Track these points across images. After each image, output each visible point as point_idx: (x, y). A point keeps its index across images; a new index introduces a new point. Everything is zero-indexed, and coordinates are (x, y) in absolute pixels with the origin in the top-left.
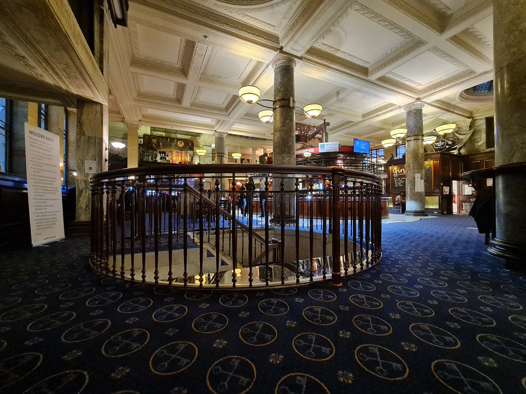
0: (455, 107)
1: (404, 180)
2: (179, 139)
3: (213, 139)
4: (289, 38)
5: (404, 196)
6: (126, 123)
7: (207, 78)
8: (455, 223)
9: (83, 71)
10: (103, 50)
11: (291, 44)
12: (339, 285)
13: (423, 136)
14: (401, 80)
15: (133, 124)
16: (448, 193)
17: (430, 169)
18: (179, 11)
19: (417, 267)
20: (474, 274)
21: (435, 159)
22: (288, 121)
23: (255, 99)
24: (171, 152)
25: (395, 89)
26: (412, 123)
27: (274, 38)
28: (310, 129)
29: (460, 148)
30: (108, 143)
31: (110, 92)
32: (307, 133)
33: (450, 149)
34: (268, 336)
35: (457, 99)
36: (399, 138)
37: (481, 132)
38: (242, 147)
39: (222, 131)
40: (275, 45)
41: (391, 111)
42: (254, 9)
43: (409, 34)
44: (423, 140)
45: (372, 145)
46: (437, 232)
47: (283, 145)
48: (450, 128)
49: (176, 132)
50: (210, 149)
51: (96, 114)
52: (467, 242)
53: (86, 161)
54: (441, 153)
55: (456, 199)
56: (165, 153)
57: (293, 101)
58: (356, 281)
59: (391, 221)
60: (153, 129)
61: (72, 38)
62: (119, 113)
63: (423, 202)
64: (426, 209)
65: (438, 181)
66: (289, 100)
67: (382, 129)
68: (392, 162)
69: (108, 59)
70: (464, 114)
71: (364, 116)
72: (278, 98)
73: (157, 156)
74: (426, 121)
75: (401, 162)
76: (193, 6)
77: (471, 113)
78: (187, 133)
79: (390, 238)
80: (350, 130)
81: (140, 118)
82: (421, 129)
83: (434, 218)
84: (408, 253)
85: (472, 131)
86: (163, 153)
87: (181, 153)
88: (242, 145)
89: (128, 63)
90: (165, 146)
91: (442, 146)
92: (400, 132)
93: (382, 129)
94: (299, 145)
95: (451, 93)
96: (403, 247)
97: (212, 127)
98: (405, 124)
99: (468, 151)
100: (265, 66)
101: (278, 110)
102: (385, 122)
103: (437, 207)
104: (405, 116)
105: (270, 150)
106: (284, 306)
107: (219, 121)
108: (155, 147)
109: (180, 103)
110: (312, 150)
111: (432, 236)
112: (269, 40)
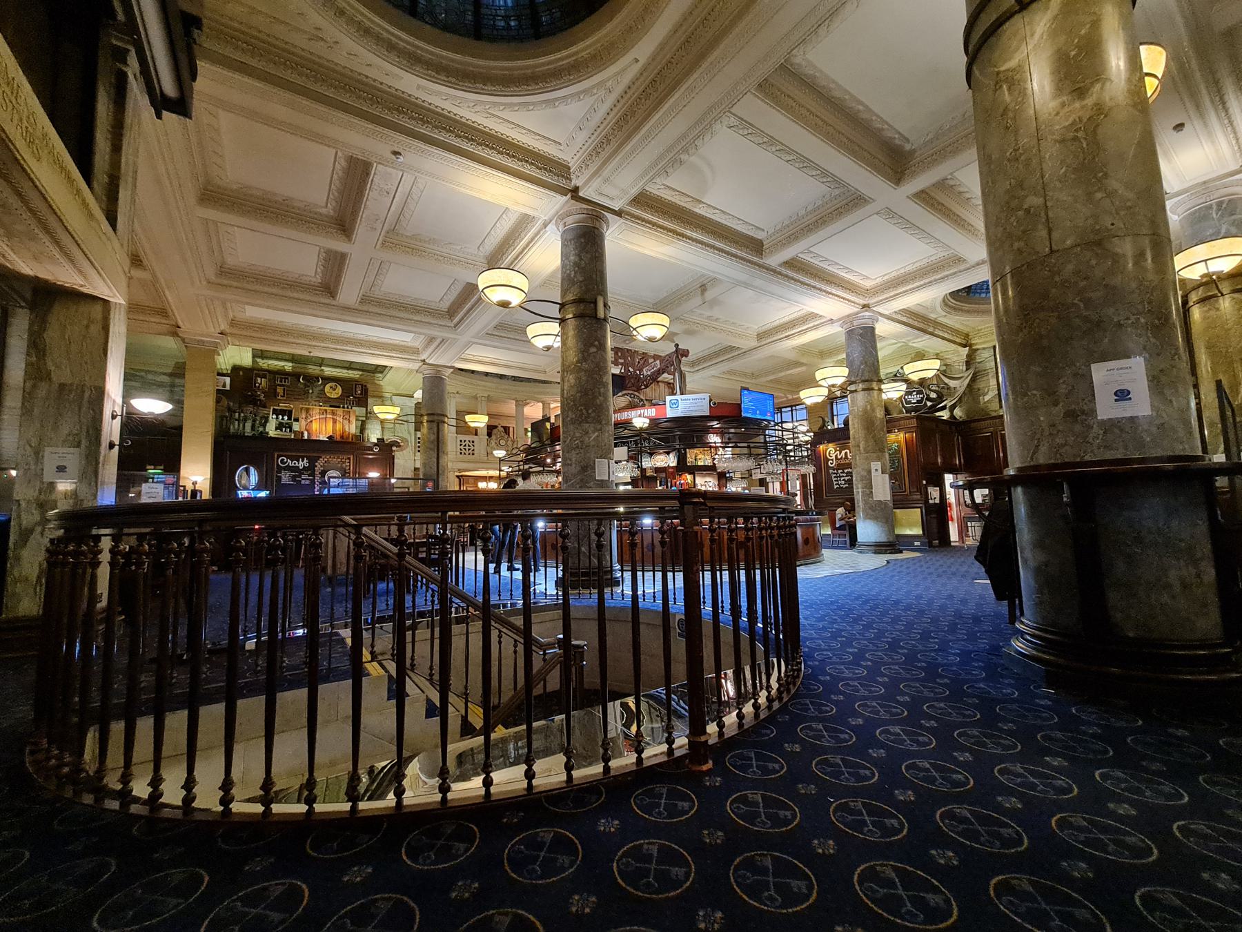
0: (936, 324)
1: (850, 474)
2: (328, 379)
3: (418, 380)
4: (592, 169)
5: (851, 509)
6: (183, 340)
7: (401, 241)
8: (953, 569)
9: (52, 221)
10: (119, 168)
11: (596, 183)
12: (705, 768)
13: (881, 381)
14: (830, 268)
15: (203, 342)
16: (937, 501)
17: (899, 451)
18: (330, 93)
19: (874, 698)
20: (987, 704)
21: (908, 430)
22: (593, 350)
23: (516, 298)
24: (307, 410)
25: (819, 285)
26: (857, 353)
27: (562, 170)
28: (646, 363)
29: (953, 408)
30: (119, 401)
31: (136, 261)
32: (641, 370)
33: (934, 409)
34: (564, 860)
35: (939, 309)
36: (833, 386)
37: (987, 375)
38: (489, 399)
39: (441, 362)
40: (562, 183)
41: (815, 328)
42: (511, 105)
43: (836, 181)
44: (880, 390)
45: (781, 397)
46: (919, 597)
47: (585, 402)
48: (926, 369)
49: (322, 362)
50: (410, 404)
51: (87, 327)
52: (977, 620)
53: (48, 450)
54: (917, 418)
55: (954, 512)
56: (289, 413)
57: (605, 305)
58: (745, 752)
59: (826, 573)
60: (258, 354)
61: (20, 144)
62: (163, 312)
63: (889, 522)
64: (898, 536)
65: (916, 476)
66: (595, 303)
67: (798, 364)
68: (822, 435)
69: (135, 186)
70: (955, 339)
71: (760, 336)
72: (570, 297)
73: (267, 420)
74: (884, 350)
75: (841, 436)
76: (366, 84)
77: (967, 335)
78: (350, 366)
79: (821, 619)
80: (736, 365)
81: (224, 326)
82: (876, 371)
83: (913, 559)
84: (859, 657)
85: (971, 371)
86: (283, 412)
87: (333, 413)
88: (492, 394)
89: (192, 200)
90: (291, 395)
91: (918, 402)
92: (834, 375)
93: (798, 364)
94: (622, 400)
95: (927, 297)
96: (848, 643)
97: (416, 351)
98: (844, 356)
99: (968, 413)
100: (539, 224)
101: (571, 324)
102: (804, 350)
103: (918, 531)
104: (842, 339)
105: (555, 408)
106: (570, 849)
107: (431, 340)
108: (262, 397)
109: (334, 297)
110: (651, 412)
111: (908, 608)
112: (547, 170)
